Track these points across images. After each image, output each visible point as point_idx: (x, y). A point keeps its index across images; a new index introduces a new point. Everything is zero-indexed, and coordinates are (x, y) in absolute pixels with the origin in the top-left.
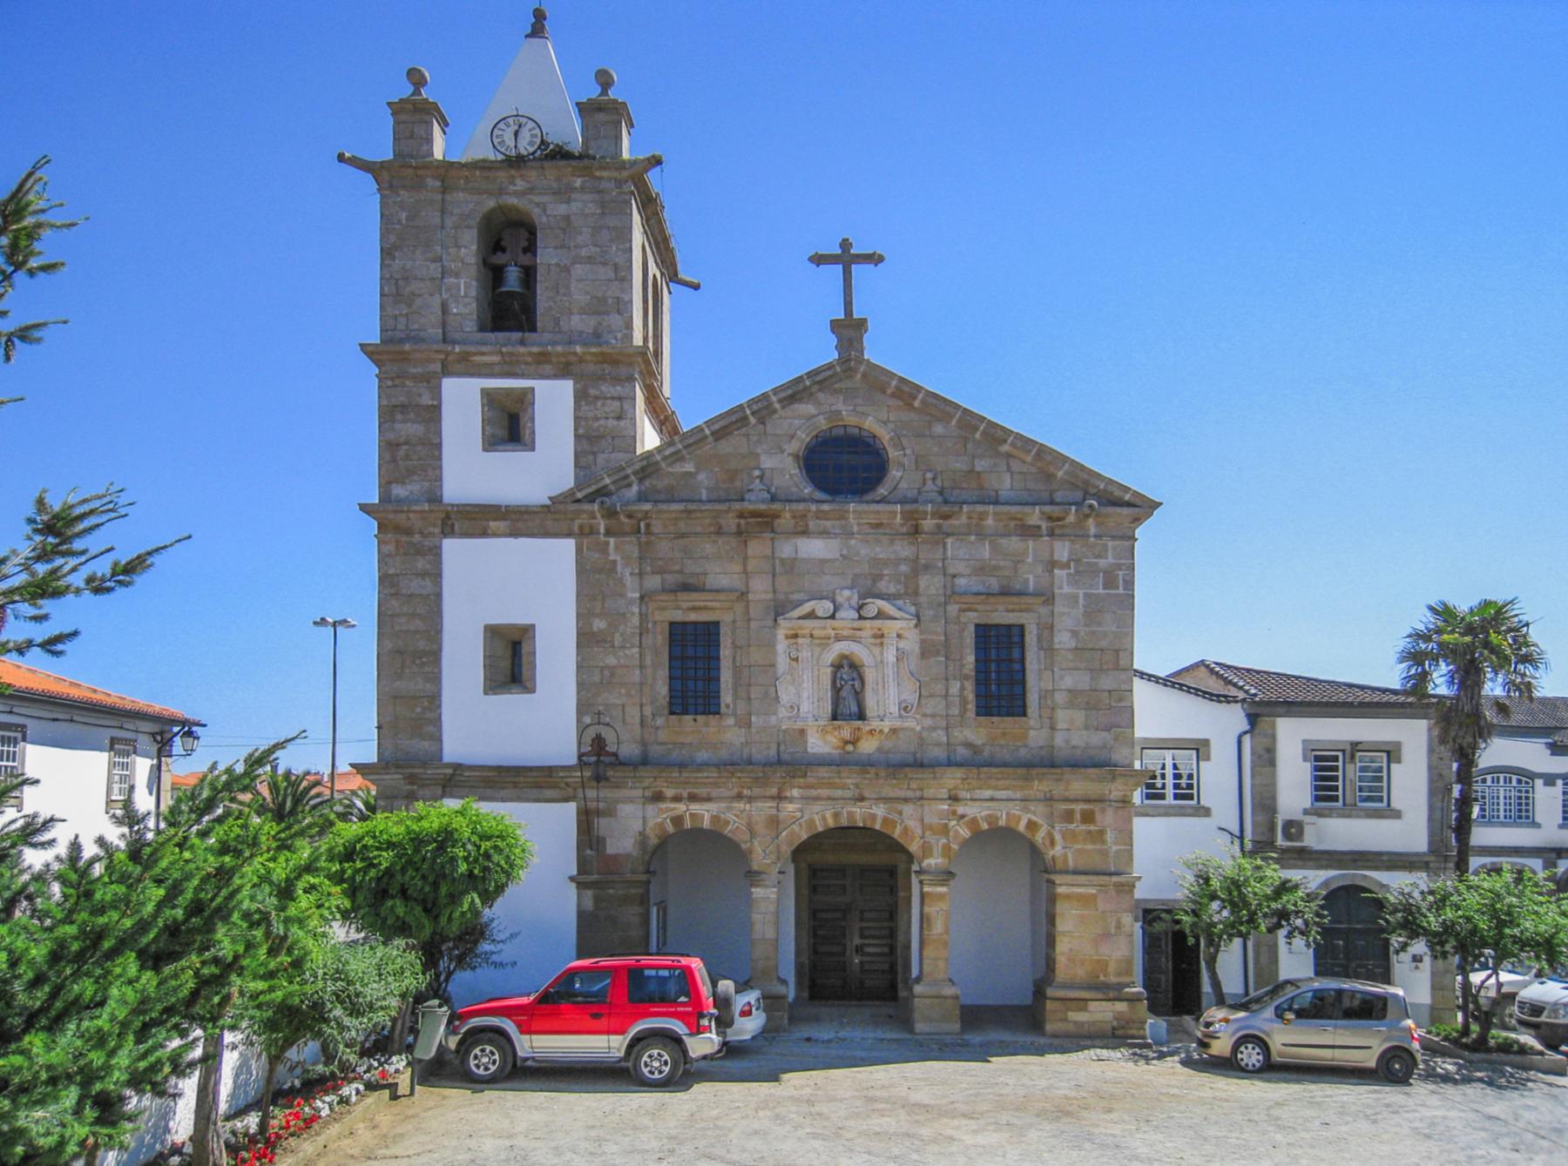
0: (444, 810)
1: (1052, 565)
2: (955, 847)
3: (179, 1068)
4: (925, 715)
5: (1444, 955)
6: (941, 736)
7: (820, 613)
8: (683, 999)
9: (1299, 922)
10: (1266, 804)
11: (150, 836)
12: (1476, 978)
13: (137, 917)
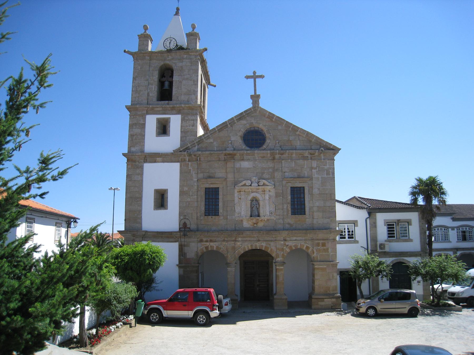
0: (142, 245)
1: (312, 168)
2: (285, 254)
3: (75, 316)
4: (277, 215)
5: (426, 280)
6: (281, 221)
7: (247, 184)
8: (208, 301)
9: (385, 273)
10: (374, 239)
11: (65, 250)
12: (436, 286)
13: (62, 273)
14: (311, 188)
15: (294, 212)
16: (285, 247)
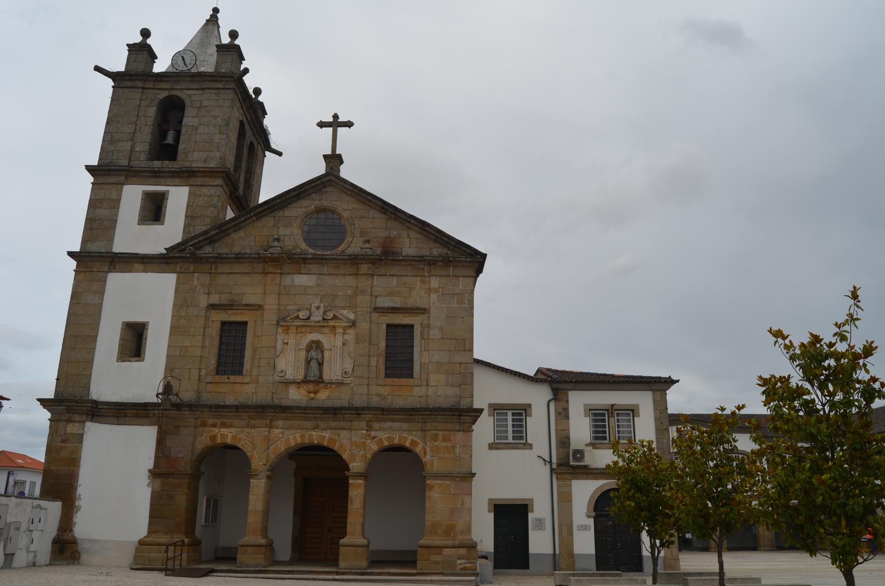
10: (564, 441)
14: (426, 327)
15: (390, 373)
16: (369, 441)
